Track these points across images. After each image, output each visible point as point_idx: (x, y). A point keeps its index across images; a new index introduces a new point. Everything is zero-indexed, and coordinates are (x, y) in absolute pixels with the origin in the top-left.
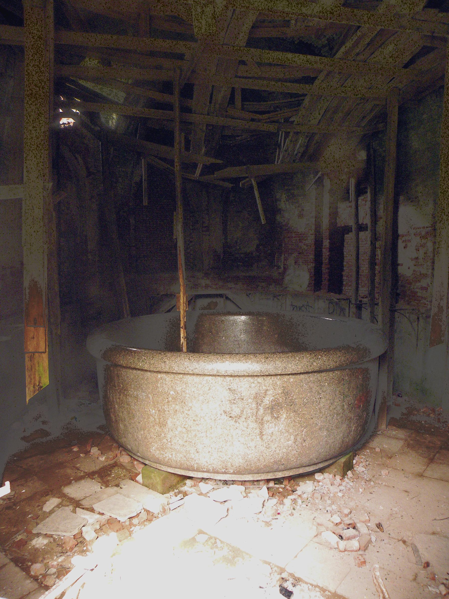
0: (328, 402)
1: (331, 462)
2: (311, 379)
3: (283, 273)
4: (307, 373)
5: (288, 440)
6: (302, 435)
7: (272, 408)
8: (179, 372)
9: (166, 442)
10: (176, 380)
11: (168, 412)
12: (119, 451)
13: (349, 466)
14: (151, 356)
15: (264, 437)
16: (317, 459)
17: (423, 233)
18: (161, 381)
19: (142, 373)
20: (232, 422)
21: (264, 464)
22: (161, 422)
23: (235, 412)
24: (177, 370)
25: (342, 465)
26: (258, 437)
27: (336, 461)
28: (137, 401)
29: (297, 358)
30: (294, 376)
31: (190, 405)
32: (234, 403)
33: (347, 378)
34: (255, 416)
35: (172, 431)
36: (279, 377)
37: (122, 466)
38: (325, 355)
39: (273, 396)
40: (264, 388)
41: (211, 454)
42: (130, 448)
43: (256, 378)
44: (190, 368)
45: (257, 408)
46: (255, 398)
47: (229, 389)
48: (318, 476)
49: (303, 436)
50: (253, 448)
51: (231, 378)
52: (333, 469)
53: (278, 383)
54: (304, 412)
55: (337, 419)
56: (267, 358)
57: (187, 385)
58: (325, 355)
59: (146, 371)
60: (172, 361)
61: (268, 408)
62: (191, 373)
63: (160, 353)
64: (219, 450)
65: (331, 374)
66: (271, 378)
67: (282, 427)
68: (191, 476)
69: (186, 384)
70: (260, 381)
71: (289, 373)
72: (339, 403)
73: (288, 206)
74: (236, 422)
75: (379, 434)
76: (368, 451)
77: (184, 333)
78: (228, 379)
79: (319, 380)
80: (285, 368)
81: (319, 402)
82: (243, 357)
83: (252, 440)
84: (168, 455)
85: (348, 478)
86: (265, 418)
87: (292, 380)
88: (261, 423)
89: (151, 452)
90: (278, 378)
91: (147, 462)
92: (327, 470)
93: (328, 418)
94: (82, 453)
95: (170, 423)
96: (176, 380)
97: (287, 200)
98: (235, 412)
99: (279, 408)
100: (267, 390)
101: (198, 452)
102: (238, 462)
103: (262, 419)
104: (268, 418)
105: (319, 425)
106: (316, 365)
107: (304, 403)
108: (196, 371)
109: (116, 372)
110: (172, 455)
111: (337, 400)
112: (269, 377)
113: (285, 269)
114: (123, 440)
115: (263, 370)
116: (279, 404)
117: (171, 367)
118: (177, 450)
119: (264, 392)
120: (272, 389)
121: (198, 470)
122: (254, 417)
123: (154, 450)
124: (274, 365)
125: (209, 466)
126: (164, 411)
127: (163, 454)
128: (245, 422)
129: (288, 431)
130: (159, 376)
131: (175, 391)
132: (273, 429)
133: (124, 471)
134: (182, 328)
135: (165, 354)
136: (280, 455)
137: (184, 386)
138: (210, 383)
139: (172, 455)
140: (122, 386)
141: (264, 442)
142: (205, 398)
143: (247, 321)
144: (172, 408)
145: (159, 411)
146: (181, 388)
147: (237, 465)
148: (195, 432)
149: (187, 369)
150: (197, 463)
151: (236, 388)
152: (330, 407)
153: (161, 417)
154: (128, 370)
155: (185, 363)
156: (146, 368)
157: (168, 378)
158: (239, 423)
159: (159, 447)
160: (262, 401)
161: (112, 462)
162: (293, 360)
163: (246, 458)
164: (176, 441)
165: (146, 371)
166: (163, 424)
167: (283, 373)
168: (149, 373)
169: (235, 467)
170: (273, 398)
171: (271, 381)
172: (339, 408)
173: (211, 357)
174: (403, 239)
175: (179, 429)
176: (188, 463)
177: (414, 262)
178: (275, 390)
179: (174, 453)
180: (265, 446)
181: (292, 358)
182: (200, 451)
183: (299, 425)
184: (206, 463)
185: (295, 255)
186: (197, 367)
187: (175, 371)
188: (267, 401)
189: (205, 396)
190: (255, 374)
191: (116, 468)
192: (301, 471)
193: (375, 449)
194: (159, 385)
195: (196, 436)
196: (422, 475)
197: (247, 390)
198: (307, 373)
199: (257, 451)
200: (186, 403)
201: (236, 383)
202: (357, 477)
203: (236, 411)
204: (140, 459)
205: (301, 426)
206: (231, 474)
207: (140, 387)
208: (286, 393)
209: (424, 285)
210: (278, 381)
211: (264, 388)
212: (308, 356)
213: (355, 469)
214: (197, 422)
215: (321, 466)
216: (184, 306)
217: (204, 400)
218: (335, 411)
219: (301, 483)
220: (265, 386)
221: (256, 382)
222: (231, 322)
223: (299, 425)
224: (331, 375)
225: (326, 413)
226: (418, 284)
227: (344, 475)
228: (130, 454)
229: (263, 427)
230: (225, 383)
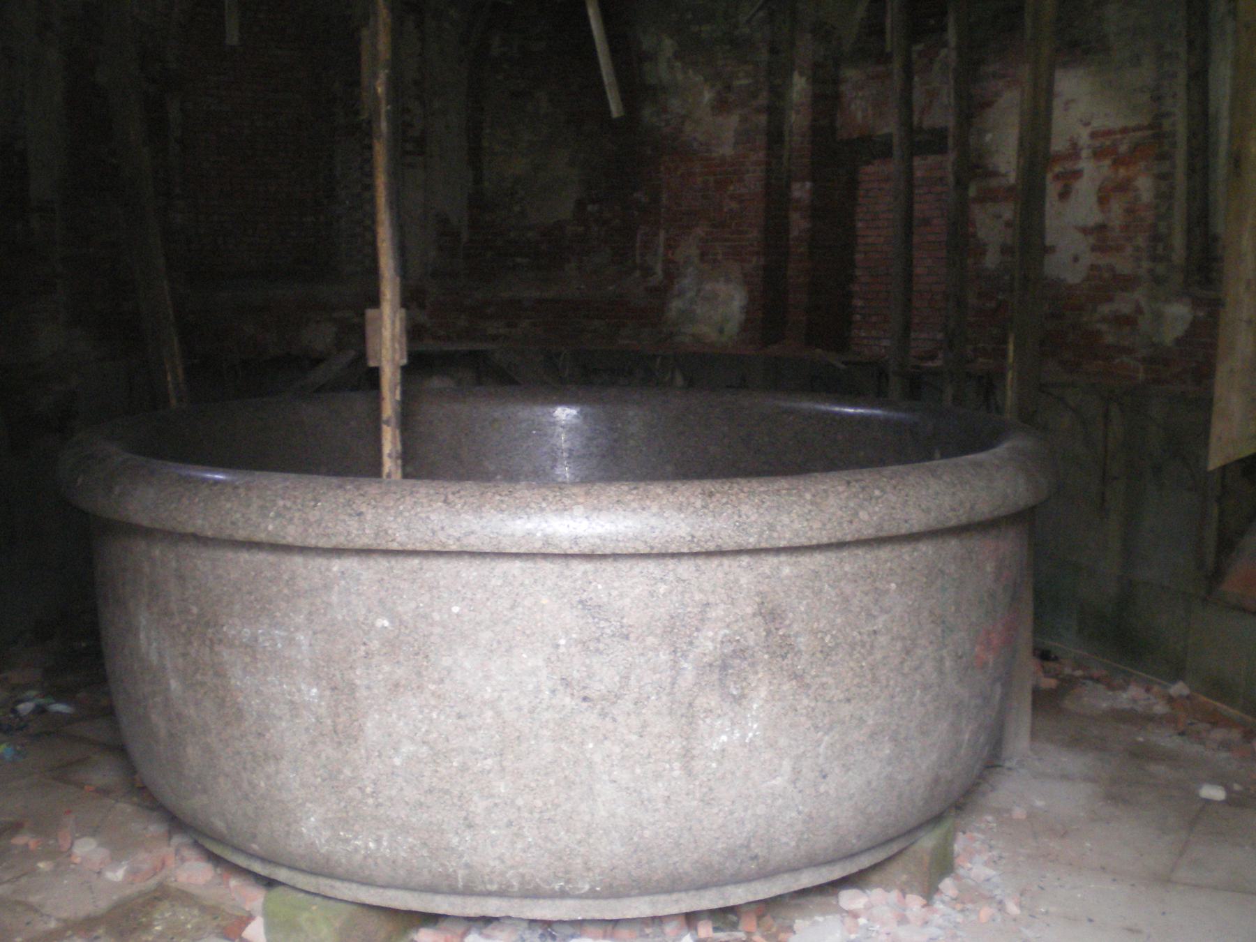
0: (899, 645)
1: (895, 848)
2: (847, 568)
3: (662, 292)
4: (840, 545)
5: (773, 774)
6: (818, 756)
7: (724, 667)
8: (410, 547)
9: (359, 796)
10: (397, 577)
11: (365, 693)
12: (172, 850)
13: (943, 865)
14: (310, 496)
15: (698, 765)
16: (859, 837)
17: (1123, 148)
18: (343, 582)
19: (272, 558)
20: (590, 718)
21: (696, 856)
22: (340, 727)
23: (601, 681)
24: (404, 539)
25: (927, 859)
26: (677, 765)
27: (905, 849)
28: (254, 658)
29: (808, 496)
30: (794, 559)
31: (446, 661)
32: (597, 650)
33: (953, 567)
34: (669, 694)
35: (380, 756)
36: (745, 560)
37: (185, 897)
38: (895, 487)
39: (728, 626)
40: (698, 597)
41: (515, 829)
42: (225, 831)
43: (671, 564)
44: (451, 531)
45: (673, 668)
46: (669, 631)
47: (581, 602)
48: (850, 899)
49: (821, 760)
50: (660, 805)
51: (589, 566)
52: (898, 872)
53: (743, 581)
54: (824, 680)
55: (923, 704)
56: (711, 495)
57: (435, 592)
58: (895, 487)
59: (288, 549)
60: (387, 509)
61: (711, 665)
62: (454, 548)
63: (340, 487)
64: (546, 815)
65: (906, 551)
66: (721, 565)
67: (754, 729)
68: (441, 911)
69: (431, 589)
70: (685, 576)
71: (783, 544)
72: (930, 649)
73: (680, 77)
74: (603, 715)
75: (1010, 769)
76: (990, 818)
77: (394, 443)
78: (580, 567)
79: (871, 573)
80: (772, 527)
81: (872, 647)
82: (629, 492)
83: (658, 776)
84: (365, 844)
85: (943, 902)
86: (701, 702)
87: (786, 571)
88: (688, 716)
89: (301, 834)
90: (744, 564)
91: (282, 874)
92: (875, 878)
93: (897, 699)
94: (41, 860)
95: (371, 727)
96: (397, 577)
97: (677, 56)
98: (601, 681)
99: (745, 665)
100: (708, 604)
101: (470, 826)
102: (609, 852)
103: (690, 705)
104: (711, 700)
105: (870, 722)
106: (869, 519)
107: (826, 649)
108: (473, 543)
109: (174, 564)
110: (378, 841)
111: (923, 642)
112: (715, 562)
113: (670, 276)
114: (193, 804)
115: (699, 534)
116: (741, 653)
117: (380, 532)
118: (399, 823)
119: (696, 610)
120: (725, 596)
121: (468, 891)
122: (664, 698)
123: (313, 828)
124: (736, 518)
125: (510, 873)
126: (353, 688)
127: (347, 841)
128: (633, 716)
129: (772, 745)
130: (337, 565)
131: (394, 617)
132: (724, 738)
133: (196, 912)
134: (387, 423)
135: (358, 489)
136: (749, 827)
137: (426, 598)
138: (516, 584)
139: (378, 841)
140: (195, 610)
141: (697, 783)
142: (499, 637)
143: (575, 421)
144: (380, 677)
145: (334, 689)
146: (413, 605)
147: (604, 865)
148: (460, 758)
149: (442, 536)
150: (467, 866)
151: (605, 600)
152: (902, 663)
153: (341, 709)
154: (219, 553)
155: (433, 517)
156: (290, 540)
157: (366, 571)
158: (614, 720)
159: (330, 815)
160: (691, 643)
161: (152, 883)
162: (795, 502)
163: (636, 839)
164: (394, 793)
165: (288, 549)
166: (346, 735)
167: (764, 545)
168: (298, 560)
169: (598, 871)
170: (727, 631)
171: (720, 575)
172: (929, 666)
173: (523, 491)
174: (1057, 169)
175: (408, 748)
176: (435, 865)
177: (1091, 240)
178: (733, 604)
179: (385, 835)
180: (698, 795)
181: (790, 495)
182: (478, 820)
183: (809, 724)
184: (497, 862)
185: (700, 231)
186: (476, 527)
187: (395, 546)
188: (708, 642)
189: (497, 629)
190: (673, 548)
191: (166, 904)
192: (807, 879)
193: (1009, 811)
194: (334, 599)
195: (464, 768)
196: (1169, 881)
197: (642, 604)
198: (840, 545)
199: (672, 813)
200: (432, 657)
201: (603, 583)
202: (971, 896)
203: (605, 678)
204: (257, 867)
205: (816, 728)
206: (580, 897)
207: (263, 608)
208: (771, 615)
209: (1126, 309)
210: (743, 573)
211: (698, 596)
212: (840, 489)
213: (961, 872)
214: (469, 721)
215: (865, 862)
216: (393, 346)
217: (495, 645)
218: (918, 677)
219: (799, 924)
220: (701, 591)
221: (671, 577)
222: (524, 425)
223: (809, 724)
224: (907, 557)
225: (892, 683)
226: (1105, 309)
227: (929, 892)
228: (218, 850)
229: (694, 730)
230: (566, 584)
